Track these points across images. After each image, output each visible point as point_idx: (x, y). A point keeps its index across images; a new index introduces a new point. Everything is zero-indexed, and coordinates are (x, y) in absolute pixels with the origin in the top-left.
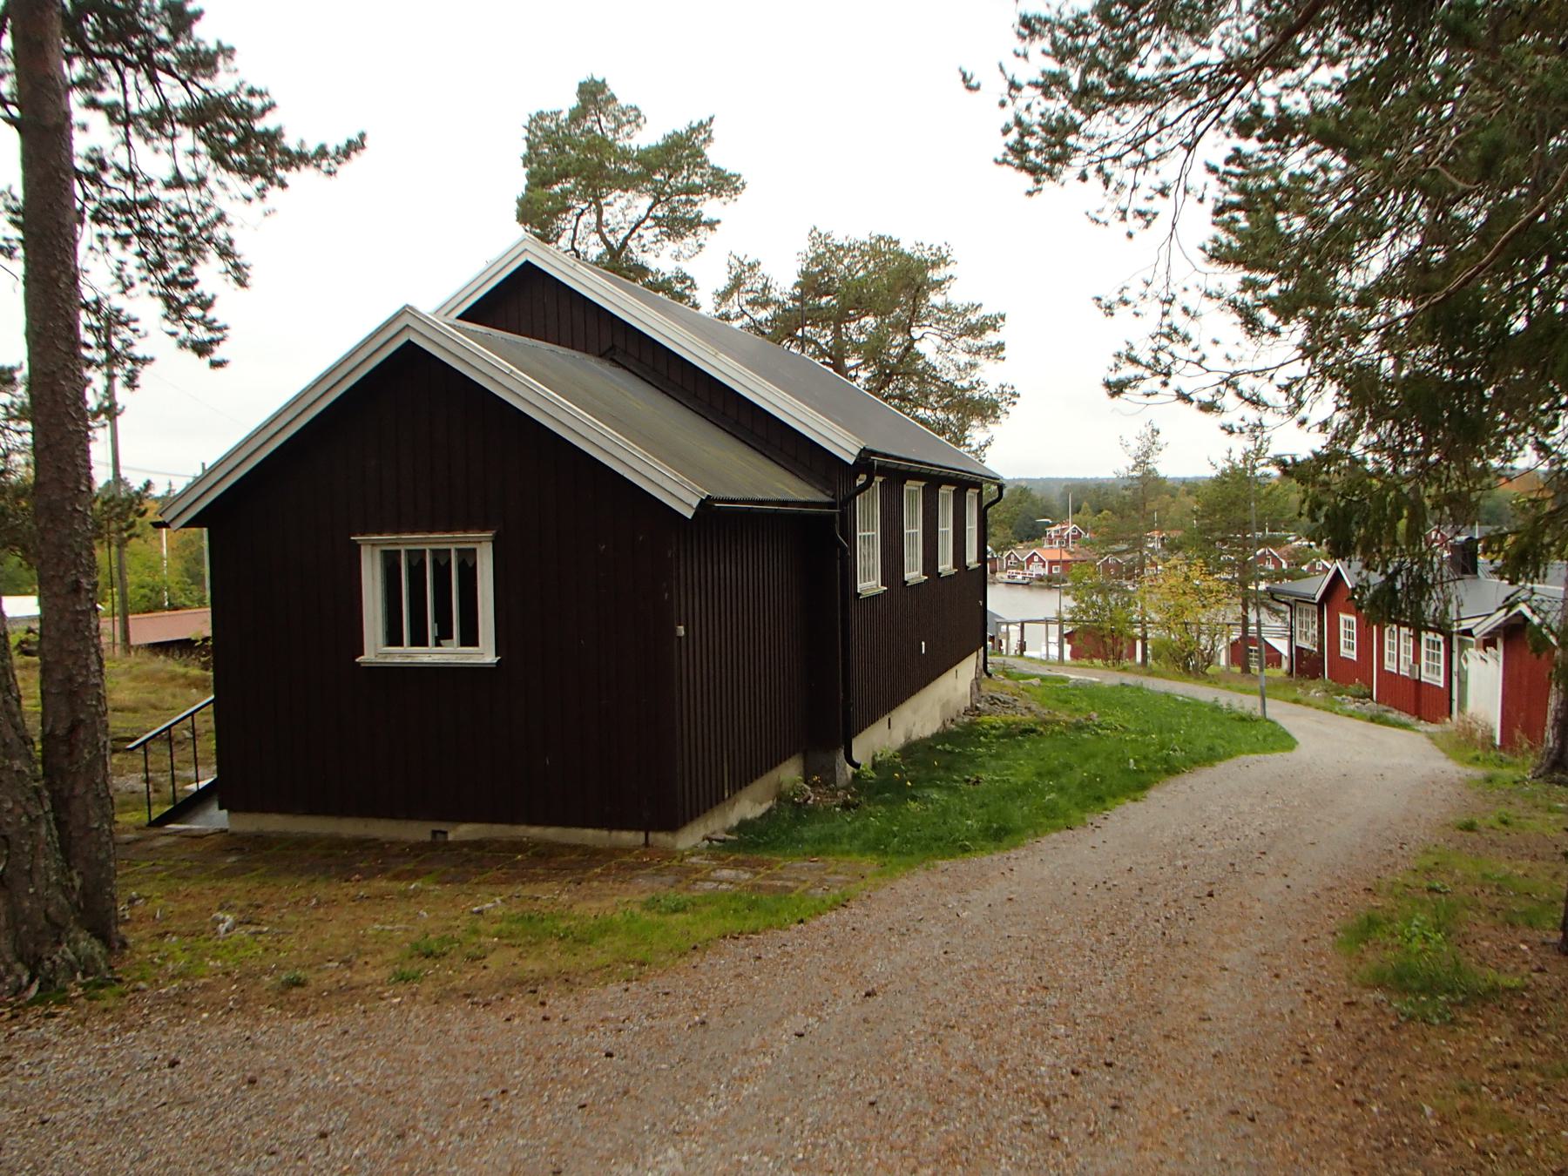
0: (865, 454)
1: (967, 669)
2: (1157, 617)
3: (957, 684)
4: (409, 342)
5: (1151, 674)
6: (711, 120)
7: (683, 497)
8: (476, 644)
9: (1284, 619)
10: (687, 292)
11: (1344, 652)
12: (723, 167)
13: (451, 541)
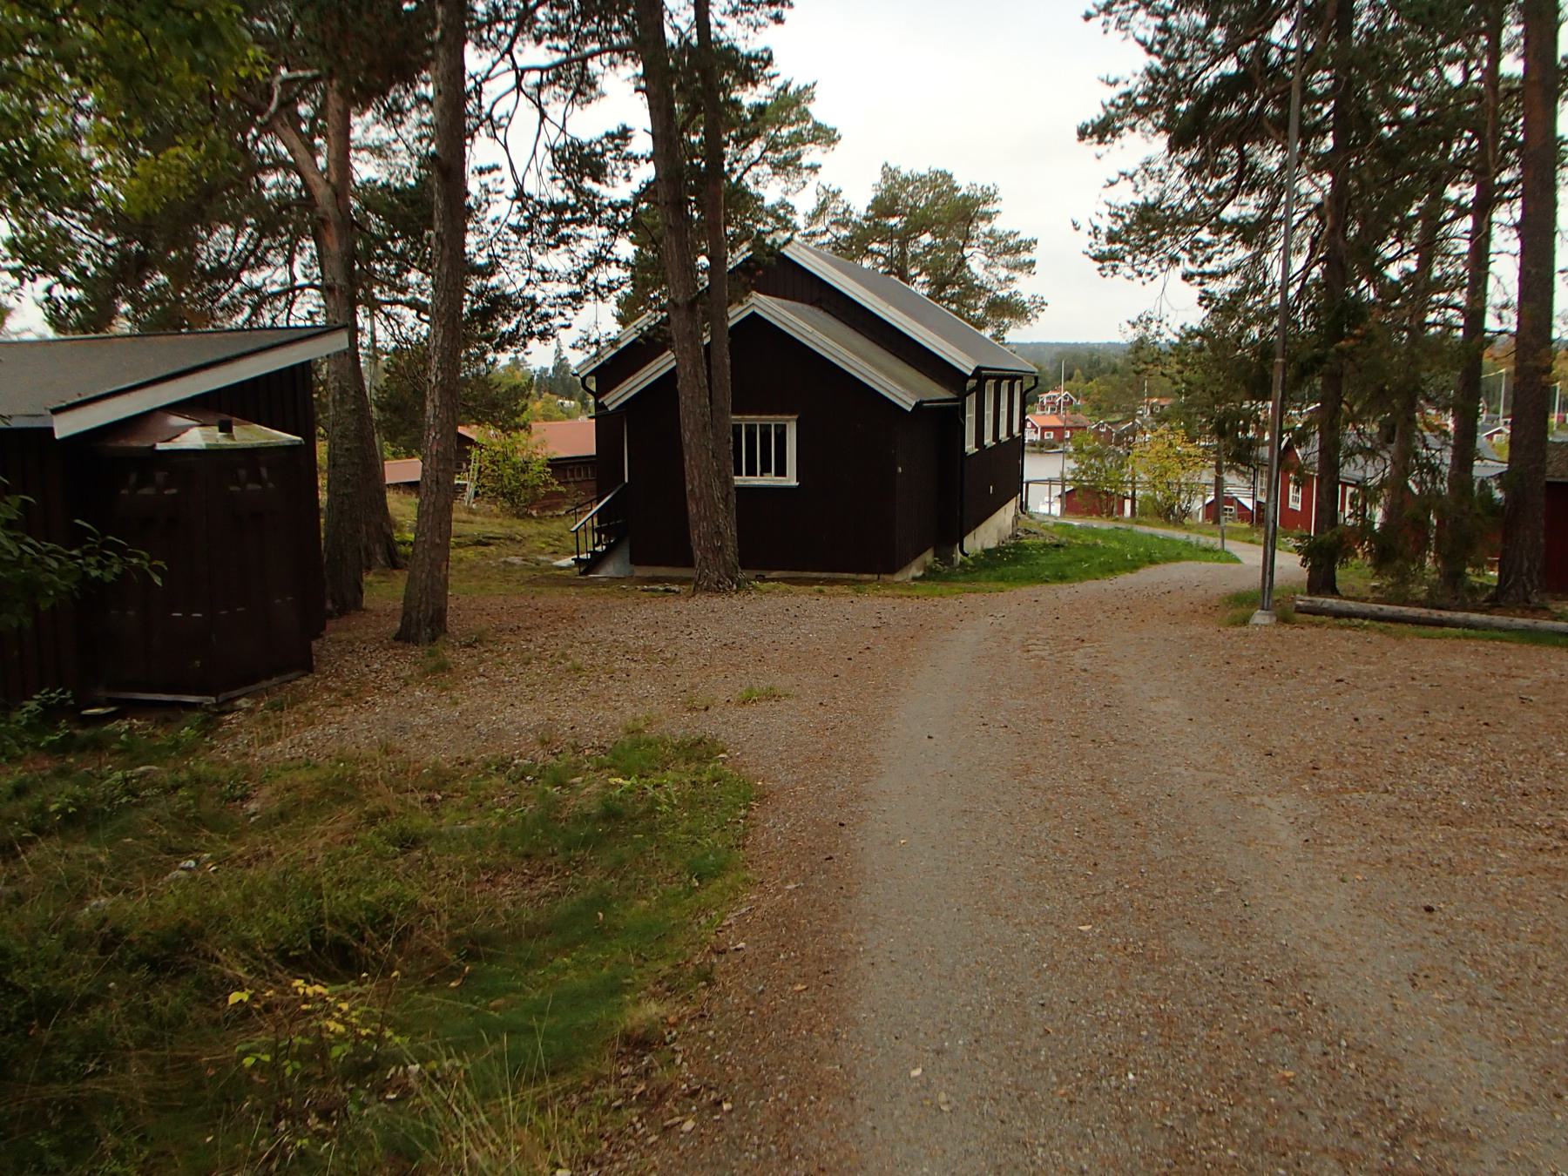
0: (978, 369)
1: (1011, 508)
2: (1145, 478)
3: (1005, 517)
4: (754, 313)
5: (1138, 523)
6: (814, 84)
7: (907, 402)
8: (784, 475)
9: (1249, 480)
10: (789, 217)
11: (1292, 505)
12: (823, 123)
13: (772, 420)
